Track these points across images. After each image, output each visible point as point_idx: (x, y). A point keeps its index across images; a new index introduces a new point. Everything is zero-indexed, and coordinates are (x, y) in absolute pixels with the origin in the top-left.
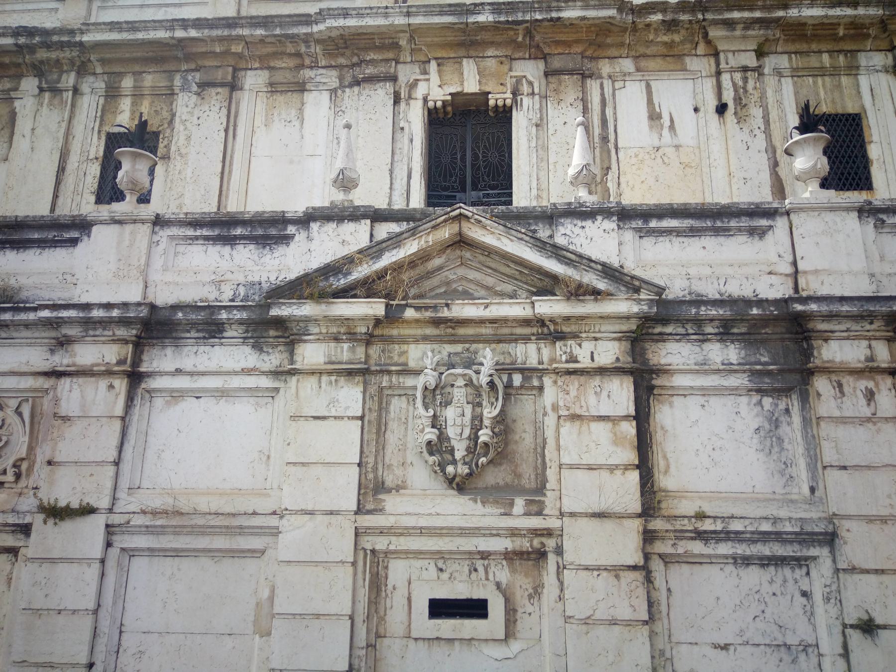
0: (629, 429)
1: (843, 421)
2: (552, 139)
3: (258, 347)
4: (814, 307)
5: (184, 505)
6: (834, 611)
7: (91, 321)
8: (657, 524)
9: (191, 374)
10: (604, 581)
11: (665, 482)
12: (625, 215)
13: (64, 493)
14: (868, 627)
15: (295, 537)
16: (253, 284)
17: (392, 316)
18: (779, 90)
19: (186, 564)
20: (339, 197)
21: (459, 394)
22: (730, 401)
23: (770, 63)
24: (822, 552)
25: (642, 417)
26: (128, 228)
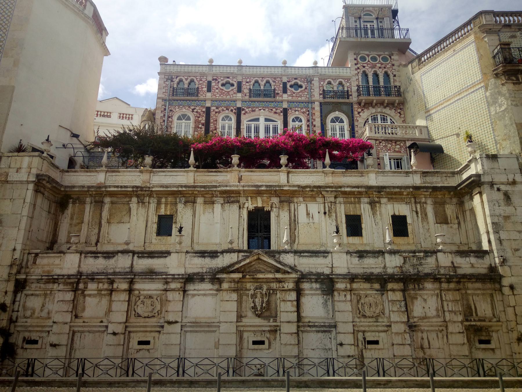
0: (295, 303)
1: (339, 301)
2: (281, 221)
3: (212, 284)
5: (198, 320)
6: (335, 342)
7: (174, 278)
8: (301, 324)
10: (289, 336)
11: (303, 314)
12: (296, 252)
13: (171, 318)
14: (341, 344)
15: (223, 327)
16: (210, 268)
17: (244, 277)
18: (340, 208)
19: (198, 334)
20: (230, 246)
21: (259, 295)
22: (317, 296)
23: (338, 200)
24: (334, 329)
25: (298, 300)
26: (180, 254)
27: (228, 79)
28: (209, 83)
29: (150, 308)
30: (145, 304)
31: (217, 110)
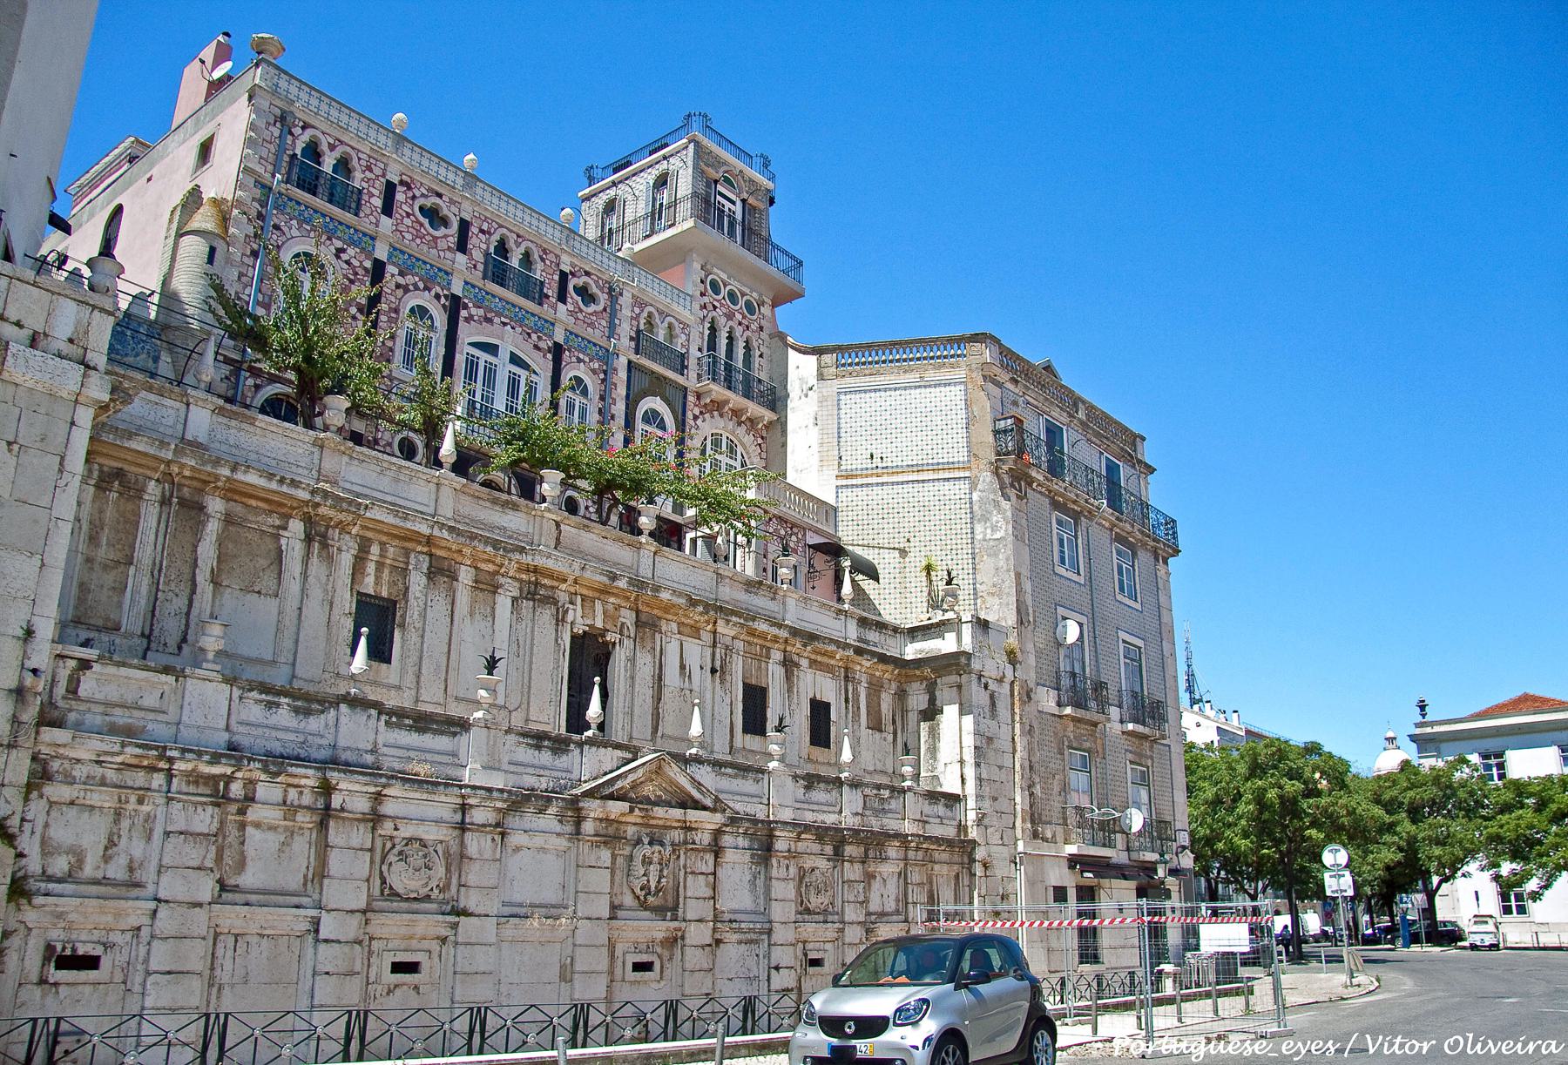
27: (438, 200)
28: (390, 189)
31: (401, 280)
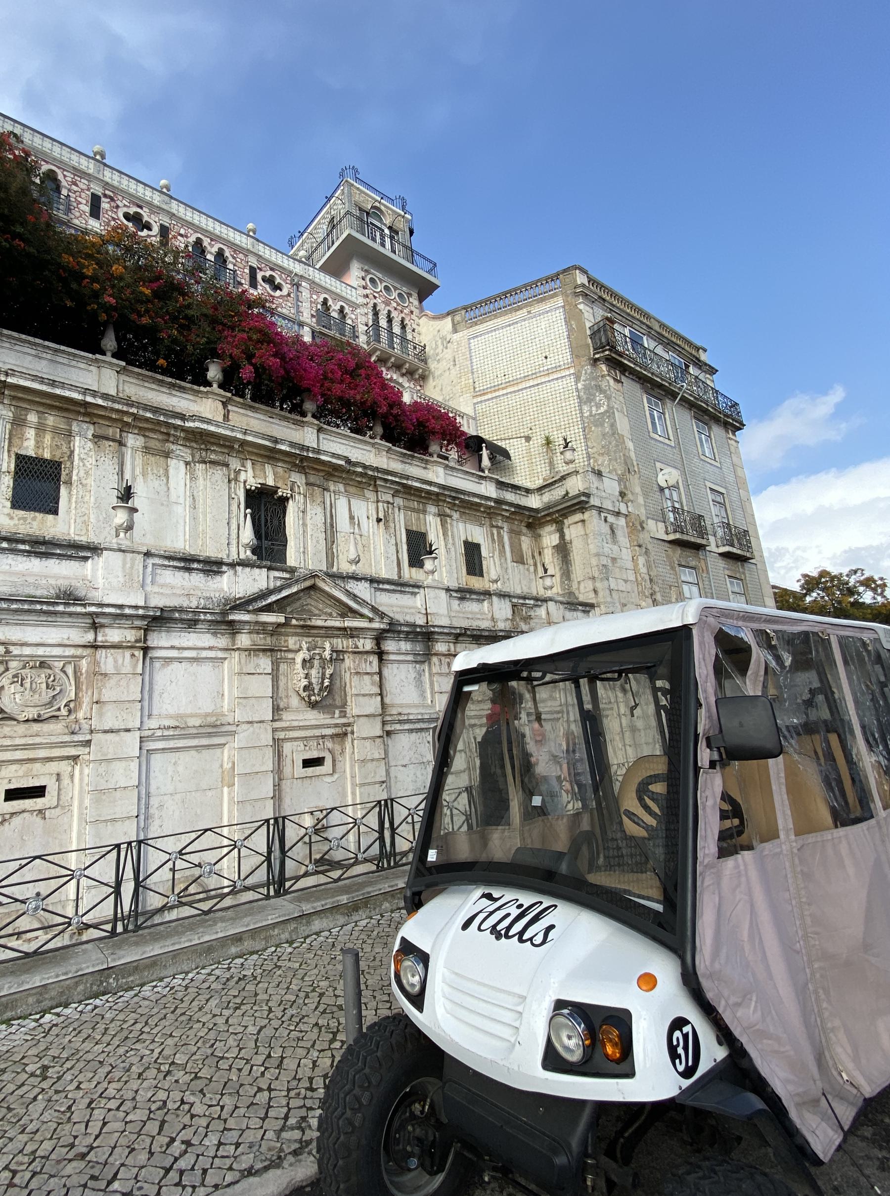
3: (215, 634)
4: (436, 629)
7: (120, 616)
9: (179, 649)
10: (368, 743)
16: (208, 598)
21: (316, 663)
22: (406, 665)
29: (46, 696)
30: (28, 685)
